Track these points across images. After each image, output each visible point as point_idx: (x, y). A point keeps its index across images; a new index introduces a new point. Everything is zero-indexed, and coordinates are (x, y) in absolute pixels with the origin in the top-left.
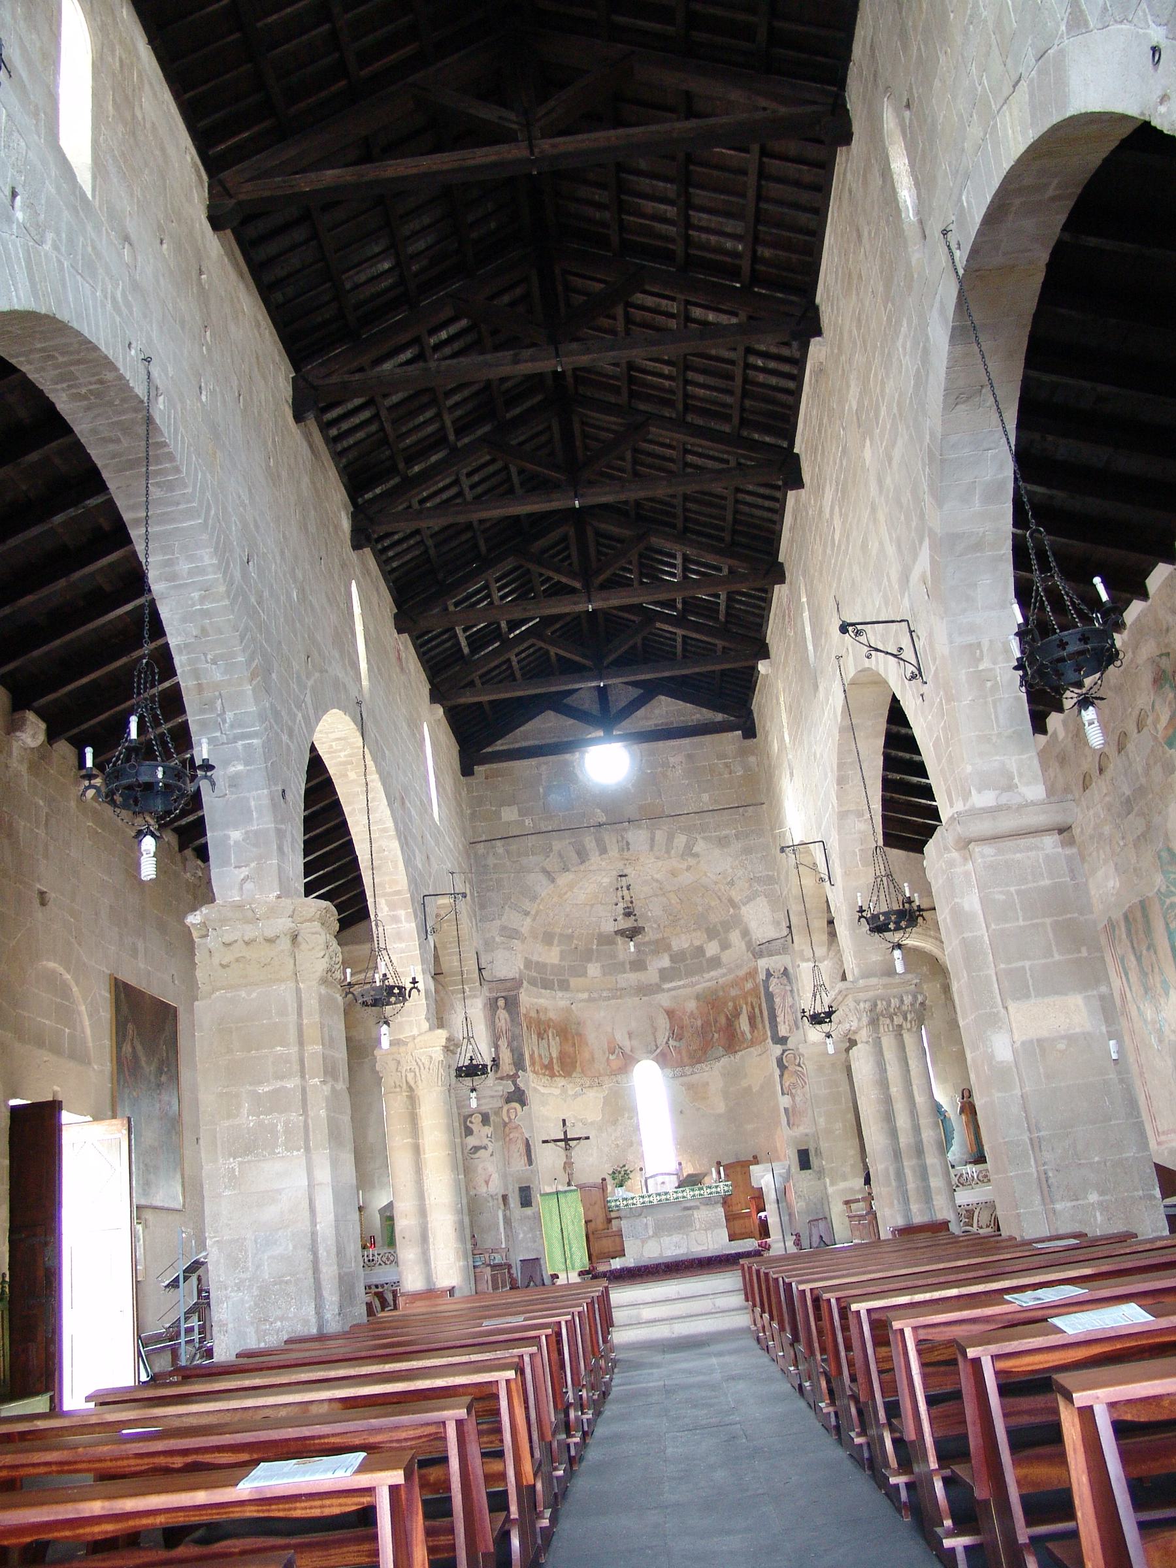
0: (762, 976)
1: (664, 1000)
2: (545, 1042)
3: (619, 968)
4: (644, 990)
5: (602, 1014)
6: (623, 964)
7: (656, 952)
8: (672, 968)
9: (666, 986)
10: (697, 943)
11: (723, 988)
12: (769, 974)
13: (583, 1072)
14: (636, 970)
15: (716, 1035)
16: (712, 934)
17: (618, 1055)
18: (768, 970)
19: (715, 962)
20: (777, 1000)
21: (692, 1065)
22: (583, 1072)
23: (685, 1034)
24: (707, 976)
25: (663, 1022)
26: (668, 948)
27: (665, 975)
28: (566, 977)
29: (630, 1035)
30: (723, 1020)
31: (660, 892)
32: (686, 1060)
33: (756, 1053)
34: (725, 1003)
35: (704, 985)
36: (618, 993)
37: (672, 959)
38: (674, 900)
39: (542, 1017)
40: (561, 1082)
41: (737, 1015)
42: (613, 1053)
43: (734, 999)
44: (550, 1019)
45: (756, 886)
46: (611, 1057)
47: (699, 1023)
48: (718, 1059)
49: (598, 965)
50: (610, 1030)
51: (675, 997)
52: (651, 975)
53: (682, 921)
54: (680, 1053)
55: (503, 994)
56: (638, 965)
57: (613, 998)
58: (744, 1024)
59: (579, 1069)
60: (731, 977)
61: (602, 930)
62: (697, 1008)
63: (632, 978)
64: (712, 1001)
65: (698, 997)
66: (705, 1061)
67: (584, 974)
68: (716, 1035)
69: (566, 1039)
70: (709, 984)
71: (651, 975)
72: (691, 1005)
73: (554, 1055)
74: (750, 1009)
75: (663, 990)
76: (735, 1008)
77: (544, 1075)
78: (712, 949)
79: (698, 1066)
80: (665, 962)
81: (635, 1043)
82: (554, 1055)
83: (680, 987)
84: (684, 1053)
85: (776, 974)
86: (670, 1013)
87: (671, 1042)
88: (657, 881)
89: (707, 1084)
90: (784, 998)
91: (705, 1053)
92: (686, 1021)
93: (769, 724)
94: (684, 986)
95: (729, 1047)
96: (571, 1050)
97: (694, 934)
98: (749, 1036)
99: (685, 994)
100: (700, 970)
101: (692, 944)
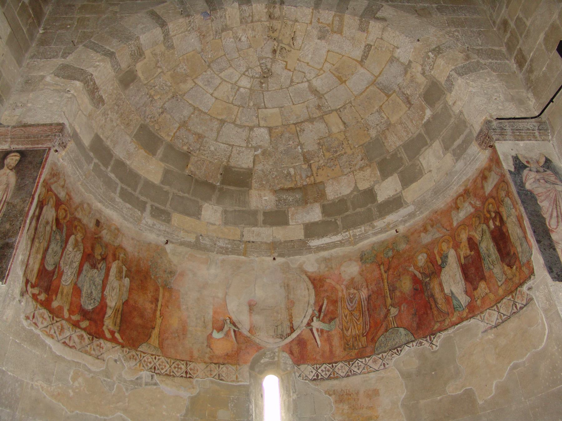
0: (508, 166)
1: (310, 262)
2: (97, 275)
3: (249, 217)
4: (276, 248)
5: (213, 271)
6: (255, 213)
7: (305, 202)
8: (323, 222)
9: (315, 243)
10: (363, 186)
11: (406, 238)
12: (520, 166)
13: (161, 346)
14: (272, 224)
15: (394, 311)
16: (386, 167)
17: (227, 334)
18: (516, 159)
19: (396, 203)
20: (545, 205)
21: (350, 361)
22: (161, 346)
23: (339, 311)
24: (379, 224)
25: (305, 295)
26: (322, 195)
27: (311, 230)
28: (168, 208)
29: (252, 307)
30: (406, 285)
31: (317, 114)
32: (339, 351)
33: (483, 326)
34: (411, 259)
35: (374, 239)
36: (243, 247)
37: (325, 211)
38: (336, 126)
39: (106, 235)
40: (113, 353)
41: (435, 268)
42: (220, 329)
43: (428, 249)
44: (120, 247)
45: (475, 58)
46: (216, 335)
47: (364, 294)
48: (397, 348)
49: (220, 209)
50: (220, 295)
51: (325, 260)
52: (294, 231)
53: (344, 158)
54: (329, 340)
55: (20, 147)
56: (277, 218)
57: (233, 252)
58: (452, 282)
59: (154, 339)
60: (419, 218)
61: (232, 163)
62: (361, 273)
63: (267, 233)
64: (386, 261)
65: (362, 258)
66: (373, 352)
67: (197, 214)
68: (394, 311)
69: (143, 288)
70: (382, 237)
71: (294, 231)
72: (352, 270)
73: (113, 302)
74: (465, 251)
75: (309, 250)
76: (431, 260)
77: (76, 325)
78: (387, 189)
79: (361, 362)
80: (315, 214)
81: (258, 319)
82: (113, 302)
83: (334, 245)
84: (336, 341)
85: (533, 166)
86: (317, 282)
87: (316, 324)
88: (314, 91)
89: (376, 392)
90: (521, 245)
91: (373, 341)
92: (342, 292)
93: (283, 414)
94: (341, 243)
95: (420, 326)
96: (149, 306)
97: (360, 175)
98: (464, 299)
99: (343, 255)
100: (368, 219)
101: (356, 188)
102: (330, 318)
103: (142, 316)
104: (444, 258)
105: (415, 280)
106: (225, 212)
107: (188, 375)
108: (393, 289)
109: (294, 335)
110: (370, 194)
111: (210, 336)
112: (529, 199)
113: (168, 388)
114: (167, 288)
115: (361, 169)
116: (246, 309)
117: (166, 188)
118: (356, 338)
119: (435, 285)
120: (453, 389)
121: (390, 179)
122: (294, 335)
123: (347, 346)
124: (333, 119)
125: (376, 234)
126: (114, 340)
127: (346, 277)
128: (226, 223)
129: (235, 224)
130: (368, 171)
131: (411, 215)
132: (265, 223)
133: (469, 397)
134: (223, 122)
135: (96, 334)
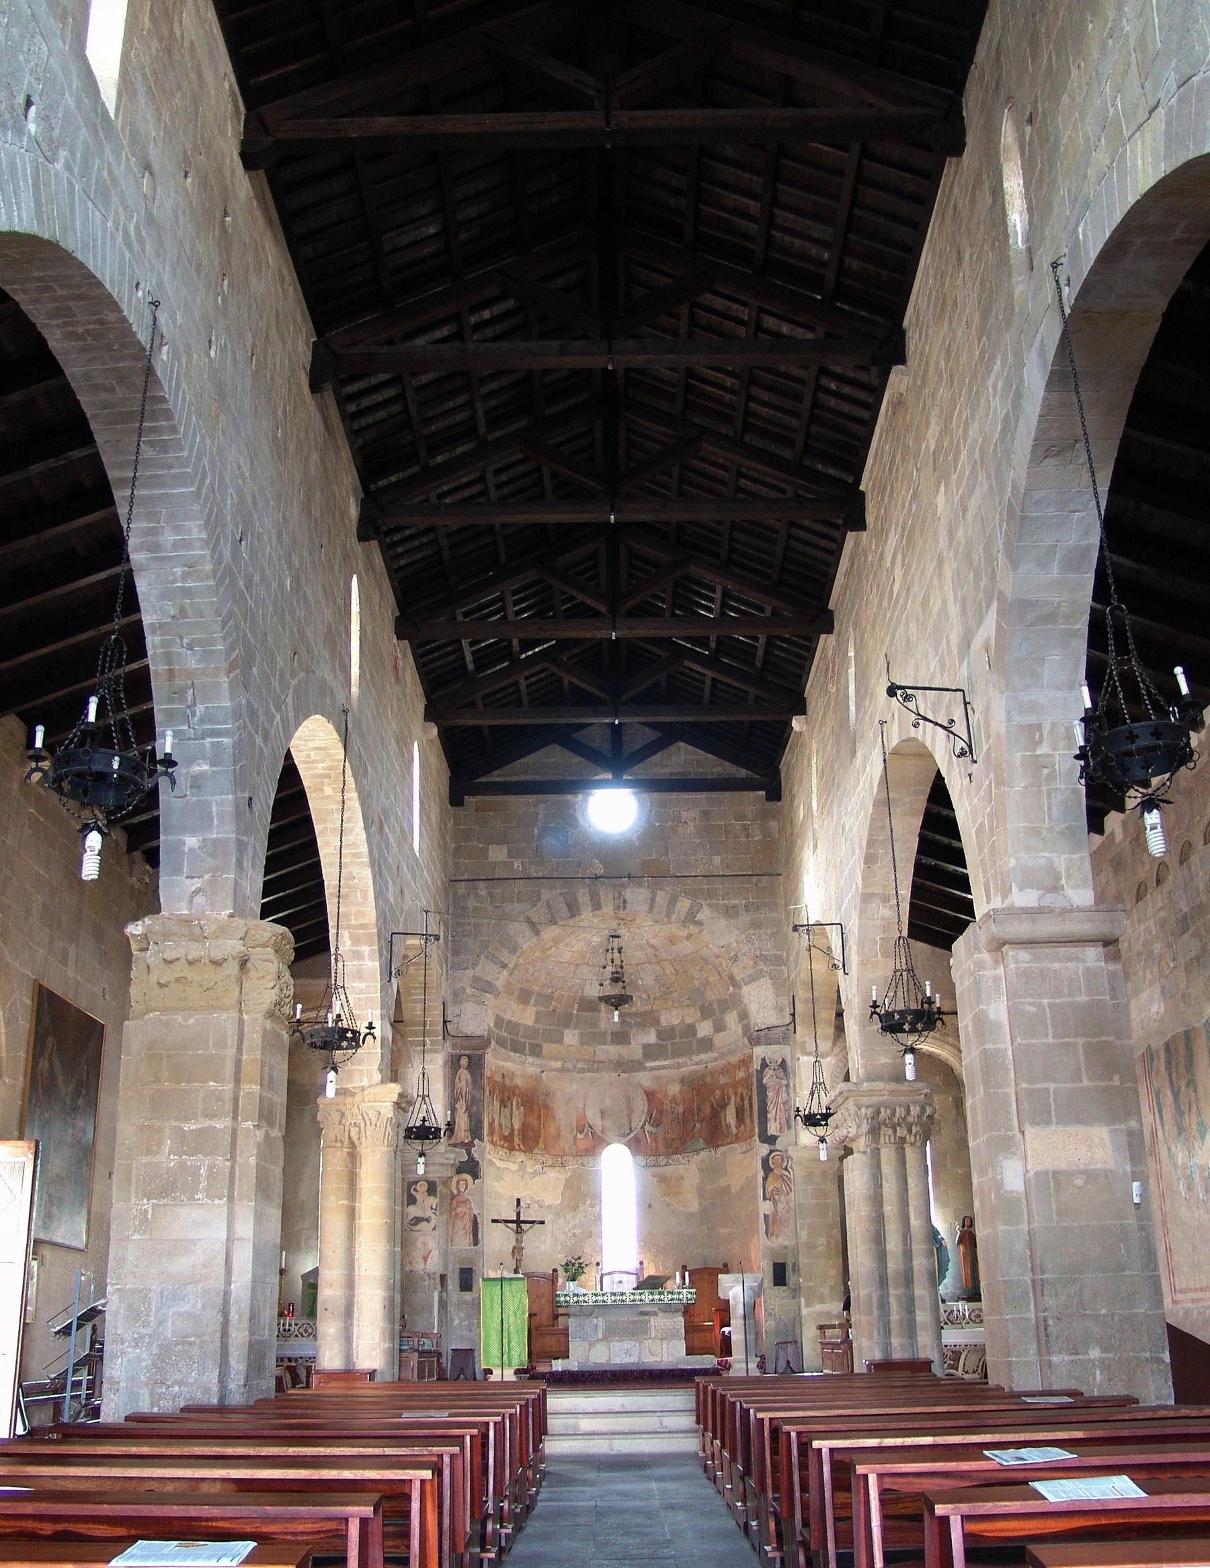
0: (757, 1065)
1: (645, 1079)
4: (623, 1066)
5: (575, 1087)
6: (604, 1034)
8: (657, 1045)
9: (649, 1064)
10: (688, 1021)
14: (618, 1043)
15: (698, 1125)
16: (706, 1012)
17: (587, 1134)
18: (764, 1060)
21: (668, 1155)
24: (695, 1058)
25: (641, 1104)
26: (656, 1022)
29: (603, 1114)
30: (707, 1110)
31: (654, 960)
32: (661, 1149)
34: (712, 1091)
36: (595, 1066)
40: (520, 1157)
41: (724, 1105)
43: (722, 1088)
45: (761, 966)
46: (579, 1136)
47: (681, 1109)
48: (697, 1151)
49: (577, 1032)
50: (581, 1106)
51: (657, 1078)
52: (634, 1050)
53: (675, 995)
54: (655, 1140)
56: (621, 1037)
58: (730, 1117)
59: (541, 1145)
62: (681, 1093)
63: (612, 1051)
64: (698, 1087)
67: (560, 1041)
68: (698, 1125)
70: (696, 1067)
71: (634, 1050)
72: (675, 1089)
75: (645, 1069)
77: (503, 1147)
80: (651, 1037)
81: (608, 1123)
83: (664, 1067)
86: (650, 1095)
87: (647, 1127)
88: (652, 946)
89: (682, 1178)
91: (683, 1143)
92: (667, 1106)
94: (669, 1067)
96: (536, 1122)
97: (686, 1011)
98: (734, 1130)
99: (669, 1075)
100: (689, 1051)
101: (683, 1021)
102: (657, 1124)
103: (533, 1130)
104: (729, 1098)
105: (713, 1108)
106: (581, 1034)
107: (563, 1165)
108: (699, 1110)
109: (632, 1135)
110: (691, 1029)
111: (575, 1137)
112: (762, 1089)
113: (552, 1174)
114: (546, 1107)
115: (688, 1006)
116: (599, 1115)
117: (538, 1026)
118: (673, 1140)
119: (722, 1114)
120: (723, 1182)
121: (706, 1022)
122: (632, 1135)
123: (667, 1146)
124: (667, 965)
125: (694, 1064)
126: (520, 1150)
127: (671, 1094)
128: (582, 1044)
129: (589, 1045)
130: (692, 1010)
131: (715, 1059)
132: (612, 1042)
133: (729, 1187)
134: (577, 965)
135: (512, 1149)
